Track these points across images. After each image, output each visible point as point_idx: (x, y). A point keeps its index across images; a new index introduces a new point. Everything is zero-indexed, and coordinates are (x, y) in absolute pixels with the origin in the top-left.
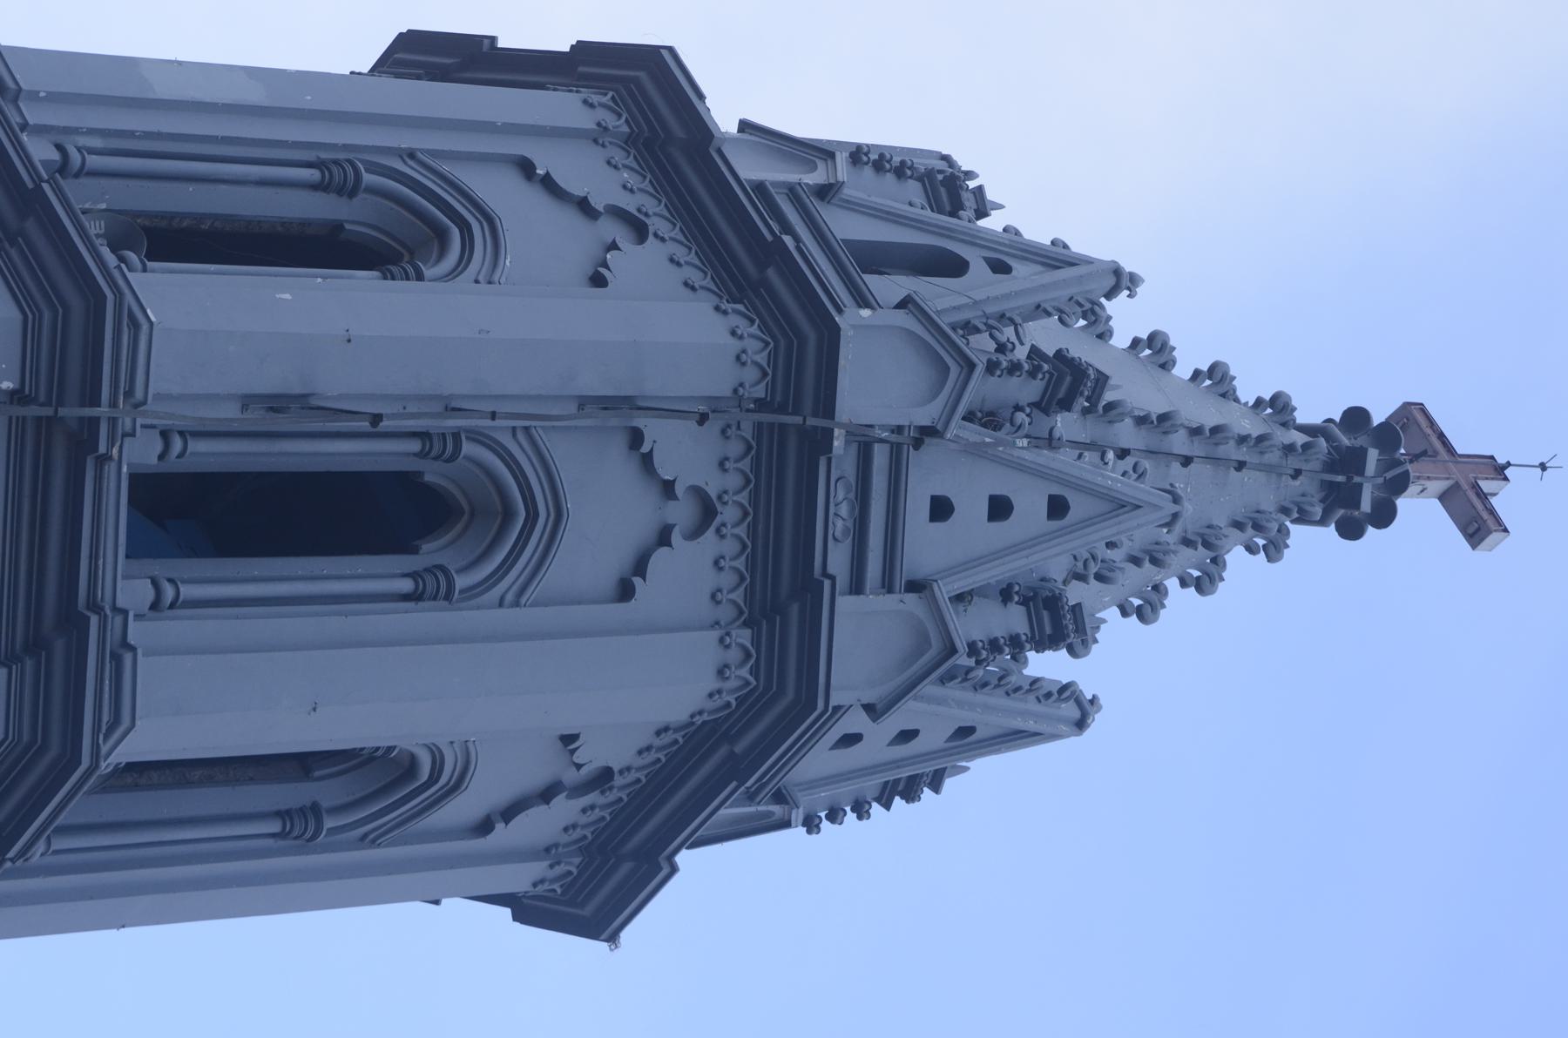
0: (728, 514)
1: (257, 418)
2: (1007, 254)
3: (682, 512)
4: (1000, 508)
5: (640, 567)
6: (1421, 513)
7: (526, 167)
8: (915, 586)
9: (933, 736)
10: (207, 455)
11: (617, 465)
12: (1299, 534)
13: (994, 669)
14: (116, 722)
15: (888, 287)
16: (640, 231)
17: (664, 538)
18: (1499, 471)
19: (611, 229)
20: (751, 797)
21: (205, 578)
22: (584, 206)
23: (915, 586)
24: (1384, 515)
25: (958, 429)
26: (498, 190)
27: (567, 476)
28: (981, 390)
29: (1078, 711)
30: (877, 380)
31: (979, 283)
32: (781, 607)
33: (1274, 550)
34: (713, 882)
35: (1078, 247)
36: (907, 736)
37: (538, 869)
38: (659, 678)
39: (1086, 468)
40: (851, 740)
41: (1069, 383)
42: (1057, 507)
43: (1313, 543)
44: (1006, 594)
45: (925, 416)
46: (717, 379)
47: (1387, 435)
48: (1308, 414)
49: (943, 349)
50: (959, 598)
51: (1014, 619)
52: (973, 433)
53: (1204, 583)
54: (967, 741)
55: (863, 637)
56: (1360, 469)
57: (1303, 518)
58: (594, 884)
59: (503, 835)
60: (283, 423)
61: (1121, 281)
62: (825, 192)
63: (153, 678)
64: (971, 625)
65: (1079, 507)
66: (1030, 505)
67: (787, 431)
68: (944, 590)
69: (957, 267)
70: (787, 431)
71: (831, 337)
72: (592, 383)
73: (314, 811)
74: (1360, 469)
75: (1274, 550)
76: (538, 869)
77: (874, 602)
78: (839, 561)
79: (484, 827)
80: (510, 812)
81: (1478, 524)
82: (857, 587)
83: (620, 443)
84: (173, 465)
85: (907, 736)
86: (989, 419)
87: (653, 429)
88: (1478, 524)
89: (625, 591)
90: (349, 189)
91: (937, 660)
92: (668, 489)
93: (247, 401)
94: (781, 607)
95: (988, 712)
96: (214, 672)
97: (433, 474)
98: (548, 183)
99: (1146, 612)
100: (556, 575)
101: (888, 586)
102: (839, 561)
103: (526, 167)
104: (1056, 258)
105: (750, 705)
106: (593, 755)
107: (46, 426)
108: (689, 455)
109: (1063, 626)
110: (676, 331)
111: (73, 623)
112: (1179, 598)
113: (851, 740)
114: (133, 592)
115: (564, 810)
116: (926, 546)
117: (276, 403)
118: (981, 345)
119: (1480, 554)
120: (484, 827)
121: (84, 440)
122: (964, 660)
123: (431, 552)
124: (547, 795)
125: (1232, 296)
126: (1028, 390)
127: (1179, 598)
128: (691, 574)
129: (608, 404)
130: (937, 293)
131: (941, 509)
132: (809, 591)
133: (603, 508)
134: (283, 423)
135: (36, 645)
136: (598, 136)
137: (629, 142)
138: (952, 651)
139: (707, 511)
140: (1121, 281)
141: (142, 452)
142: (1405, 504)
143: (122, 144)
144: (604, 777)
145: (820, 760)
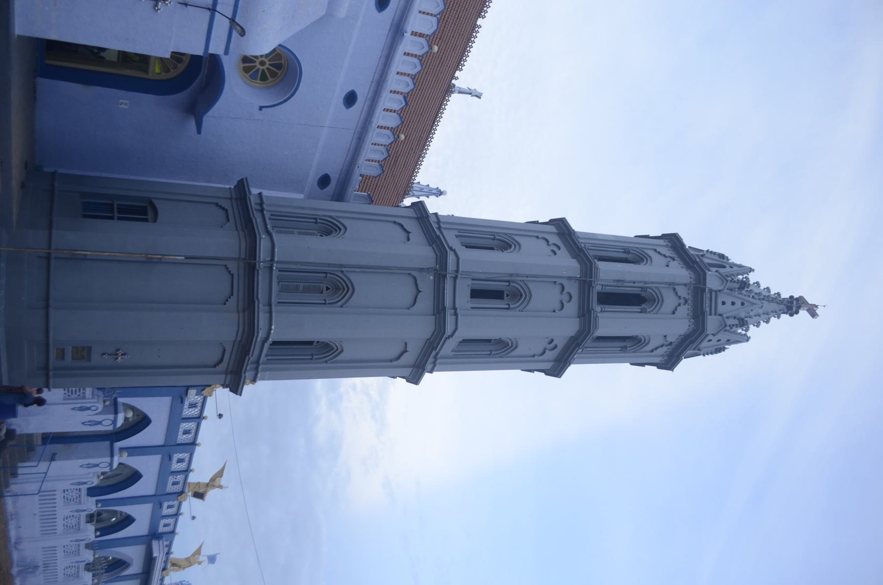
0: (690, 302)
1: (615, 284)
2: (732, 265)
3: (682, 301)
4: (733, 304)
5: (676, 309)
6: (803, 313)
7: (655, 250)
8: (720, 315)
9: (724, 341)
10: (609, 289)
11: (672, 293)
12: (782, 315)
13: (734, 330)
14: (596, 328)
15: (714, 269)
16: (674, 259)
17: (679, 305)
18: (817, 306)
19: (669, 259)
20: (694, 349)
21: (608, 308)
22: (665, 256)
23: (720, 315)
24: (797, 313)
25: (726, 291)
26: (651, 253)
27: (664, 294)
28: (729, 285)
29: (748, 339)
30: (712, 282)
31: (728, 269)
32: (699, 316)
33: (779, 317)
34: (686, 364)
35: (744, 264)
36: (719, 340)
37: (661, 359)
38: (680, 326)
39: (746, 298)
40: (710, 340)
41: (744, 284)
42: (743, 304)
43: (784, 317)
44: (735, 318)
45: (720, 288)
46: (687, 281)
47: (797, 299)
48: (783, 296)
49: (724, 278)
50: (727, 318)
51: (736, 322)
52: (728, 291)
53: (767, 322)
54: (729, 342)
55: (712, 323)
56: (793, 305)
57: (784, 313)
58: (669, 363)
59: (655, 352)
60: (620, 284)
61: (751, 270)
62: (702, 256)
63: (601, 322)
64: (730, 322)
65: (746, 304)
66: (738, 303)
67: (699, 290)
68: (725, 316)
69: (725, 267)
70: (699, 290)
71: (705, 274)
72: (667, 280)
73: (626, 347)
74: (793, 305)
75: (779, 317)
76: (661, 359)
77: (713, 317)
78: (708, 309)
79: (652, 351)
80: (656, 349)
81: (813, 314)
82: (710, 314)
83: (672, 291)
84: (603, 291)
85: (719, 340)
86: (731, 290)
87: (676, 287)
88: (813, 314)
89: (674, 313)
90: (629, 253)
91: (723, 327)
92: (680, 297)
93: (615, 281)
94: (699, 316)
95: (732, 337)
96: (612, 322)
97: (643, 294)
98: (659, 253)
99: (758, 326)
100: (662, 310)
101: (715, 314)
102: (708, 309)
103: (655, 250)
104: (740, 266)
105: (694, 332)
106: (671, 339)
107: (584, 281)
108: (683, 292)
109: (743, 323)
110: (680, 273)
111: (589, 311)
112: (763, 324)
113: (710, 340)
114: (598, 308)
115: (665, 349)
116: (721, 309)
117: (619, 281)
118: (729, 279)
119: (814, 320)
120: (652, 351)
121: (590, 285)
122: (728, 328)
123: (643, 306)
124: (662, 346)
125: (768, 277)
126: (737, 286)
127: (763, 324)
128: (684, 310)
129: (670, 284)
130: (721, 270)
131: (724, 303)
132: (703, 313)
133: (670, 301)
134: (620, 284)
135: (584, 315)
136: (666, 246)
137: (671, 247)
138: (726, 326)
139: (686, 301)
140: (751, 270)
141: (598, 288)
142: (800, 311)
143: (594, 245)
144: (671, 343)
145: (705, 344)
